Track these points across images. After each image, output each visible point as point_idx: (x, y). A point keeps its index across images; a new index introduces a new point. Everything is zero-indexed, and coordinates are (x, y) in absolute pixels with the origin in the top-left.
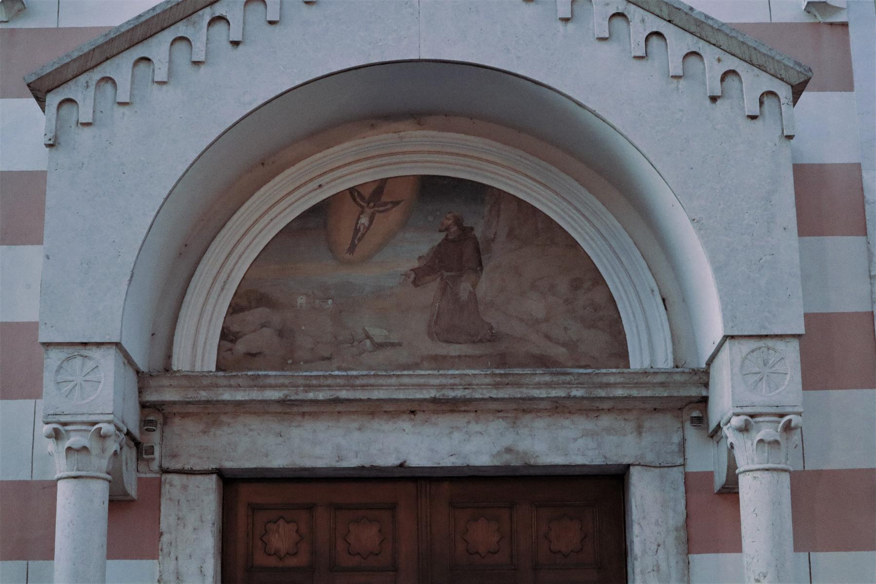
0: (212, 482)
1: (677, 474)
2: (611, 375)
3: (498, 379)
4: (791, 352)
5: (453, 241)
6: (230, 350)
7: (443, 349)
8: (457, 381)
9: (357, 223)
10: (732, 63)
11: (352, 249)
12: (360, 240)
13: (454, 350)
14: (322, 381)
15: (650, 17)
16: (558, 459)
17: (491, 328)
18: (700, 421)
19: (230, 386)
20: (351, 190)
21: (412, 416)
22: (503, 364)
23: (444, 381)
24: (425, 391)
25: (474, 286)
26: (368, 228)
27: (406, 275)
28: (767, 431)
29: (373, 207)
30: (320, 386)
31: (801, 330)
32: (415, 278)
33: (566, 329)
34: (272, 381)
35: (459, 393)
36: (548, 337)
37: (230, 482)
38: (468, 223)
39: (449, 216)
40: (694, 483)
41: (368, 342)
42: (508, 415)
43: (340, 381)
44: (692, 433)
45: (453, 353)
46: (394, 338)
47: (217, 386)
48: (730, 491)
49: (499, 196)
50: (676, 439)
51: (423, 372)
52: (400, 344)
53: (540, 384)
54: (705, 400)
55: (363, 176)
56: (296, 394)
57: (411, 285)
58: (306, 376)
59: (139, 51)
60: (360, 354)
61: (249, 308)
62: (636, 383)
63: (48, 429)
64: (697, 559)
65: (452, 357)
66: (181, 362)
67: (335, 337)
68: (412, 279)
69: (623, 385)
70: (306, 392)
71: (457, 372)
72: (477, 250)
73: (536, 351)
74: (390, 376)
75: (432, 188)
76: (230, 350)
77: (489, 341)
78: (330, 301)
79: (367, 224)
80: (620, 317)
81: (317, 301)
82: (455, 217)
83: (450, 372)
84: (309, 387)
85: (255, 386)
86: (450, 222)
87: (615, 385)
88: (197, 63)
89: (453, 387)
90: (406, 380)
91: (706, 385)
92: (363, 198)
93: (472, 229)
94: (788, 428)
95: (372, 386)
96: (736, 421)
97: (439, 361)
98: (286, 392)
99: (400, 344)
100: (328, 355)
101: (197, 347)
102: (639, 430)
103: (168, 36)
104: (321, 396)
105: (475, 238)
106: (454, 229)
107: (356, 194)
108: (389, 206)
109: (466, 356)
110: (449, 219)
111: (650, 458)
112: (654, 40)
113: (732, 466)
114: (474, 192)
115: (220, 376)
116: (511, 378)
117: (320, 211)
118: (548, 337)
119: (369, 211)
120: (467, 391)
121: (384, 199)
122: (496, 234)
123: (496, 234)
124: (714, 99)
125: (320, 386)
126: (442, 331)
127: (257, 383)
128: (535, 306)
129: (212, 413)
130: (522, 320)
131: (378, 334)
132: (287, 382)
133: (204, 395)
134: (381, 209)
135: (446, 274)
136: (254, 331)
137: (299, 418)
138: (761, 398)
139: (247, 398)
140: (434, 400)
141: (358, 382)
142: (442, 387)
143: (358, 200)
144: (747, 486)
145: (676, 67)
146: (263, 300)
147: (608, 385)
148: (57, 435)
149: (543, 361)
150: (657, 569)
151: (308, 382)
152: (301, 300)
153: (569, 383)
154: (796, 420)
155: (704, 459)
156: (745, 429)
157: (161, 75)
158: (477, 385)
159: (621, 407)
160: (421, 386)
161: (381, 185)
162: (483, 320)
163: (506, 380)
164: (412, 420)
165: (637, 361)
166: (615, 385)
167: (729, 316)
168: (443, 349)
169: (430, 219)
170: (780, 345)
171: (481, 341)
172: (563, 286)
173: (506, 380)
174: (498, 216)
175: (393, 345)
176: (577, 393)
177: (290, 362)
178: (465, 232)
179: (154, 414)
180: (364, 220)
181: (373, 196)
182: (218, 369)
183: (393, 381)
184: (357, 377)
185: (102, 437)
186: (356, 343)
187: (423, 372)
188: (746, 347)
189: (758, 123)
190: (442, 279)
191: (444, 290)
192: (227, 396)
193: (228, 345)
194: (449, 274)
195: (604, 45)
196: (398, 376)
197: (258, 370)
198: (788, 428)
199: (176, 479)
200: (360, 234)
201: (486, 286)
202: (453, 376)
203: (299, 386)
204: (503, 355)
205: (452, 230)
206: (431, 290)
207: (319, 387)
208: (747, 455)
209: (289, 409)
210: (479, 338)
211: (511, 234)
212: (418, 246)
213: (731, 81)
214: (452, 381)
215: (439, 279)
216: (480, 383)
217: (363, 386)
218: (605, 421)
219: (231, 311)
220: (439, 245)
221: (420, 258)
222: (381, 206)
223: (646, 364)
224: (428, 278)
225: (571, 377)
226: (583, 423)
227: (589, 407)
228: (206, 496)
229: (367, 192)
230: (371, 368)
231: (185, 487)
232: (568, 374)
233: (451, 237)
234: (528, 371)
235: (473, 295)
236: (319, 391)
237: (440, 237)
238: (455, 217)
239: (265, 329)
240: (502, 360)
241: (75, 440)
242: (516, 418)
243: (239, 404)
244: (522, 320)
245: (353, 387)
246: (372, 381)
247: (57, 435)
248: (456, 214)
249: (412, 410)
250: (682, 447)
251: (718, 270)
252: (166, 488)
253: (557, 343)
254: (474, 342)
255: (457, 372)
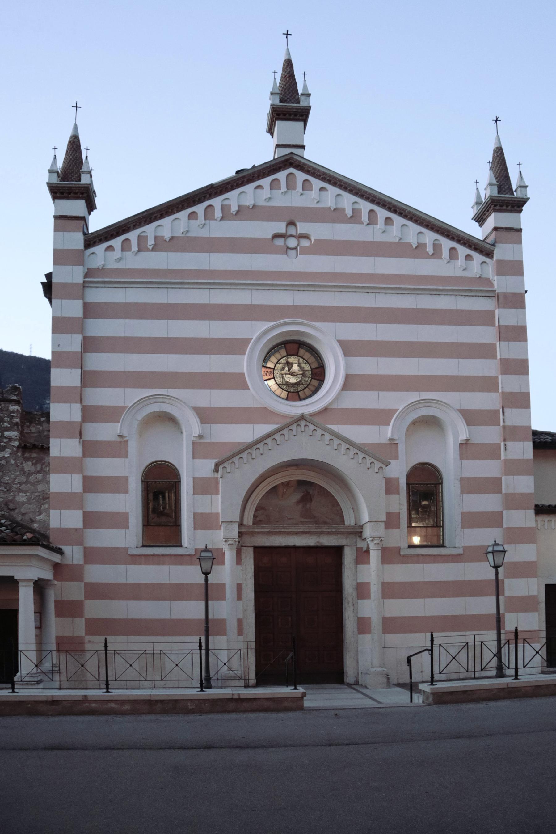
0: (252, 549)
1: (355, 548)
2: (341, 526)
4: (383, 525)
10: (373, 460)
11: (282, 497)
13: (305, 520)
15: (355, 449)
16: (329, 544)
18: (361, 537)
22: (316, 524)
28: (377, 541)
31: (385, 520)
35: (308, 530)
37: (257, 549)
40: (359, 550)
44: (358, 539)
48: (367, 551)
50: (355, 540)
54: (361, 532)
55: (285, 480)
59: (240, 456)
63: (224, 540)
64: (359, 566)
66: (245, 523)
75: (301, 483)
84: (274, 529)
88: (253, 459)
91: (362, 529)
94: (381, 541)
96: (370, 539)
97: (303, 523)
101: (249, 520)
102: (347, 538)
103: (246, 452)
104: (277, 530)
111: (349, 544)
112: (356, 455)
113: (368, 547)
114: (310, 484)
117: (274, 488)
124: (368, 468)
127: (263, 528)
129: (252, 534)
133: (251, 530)
138: (376, 534)
140: (302, 532)
144: (371, 552)
145: (360, 461)
148: (226, 541)
149: (326, 523)
150: (350, 568)
154: (383, 539)
155: (361, 545)
156: (372, 541)
157: (245, 461)
159: (342, 533)
161: (289, 482)
165: (347, 523)
167: (370, 515)
170: (380, 523)
176: (334, 530)
178: (308, 493)
179: (241, 534)
181: (287, 485)
182: (253, 524)
185: (235, 541)
188: (373, 523)
189: (378, 474)
192: (256, 530)
195: (345, 456)
198: (381, 541)
199: (245, 548)
206: (301, 506)
208: (372, 546)
209: (269, 533)
212: (297, 496)
213: (372, 464)
216: (312, 528)
218: (339, 536)
226: (335, 537)
227: (336, 533)
228: (251, 551)
231: (246, 550)
237: (302, 494)
240: (316, 523)
241: (230, 542)
243: (258, 532)
247: (226, 541)
249: (297, 533)
250: (356, 543)
251: (368, 507)
252: (242, 550)
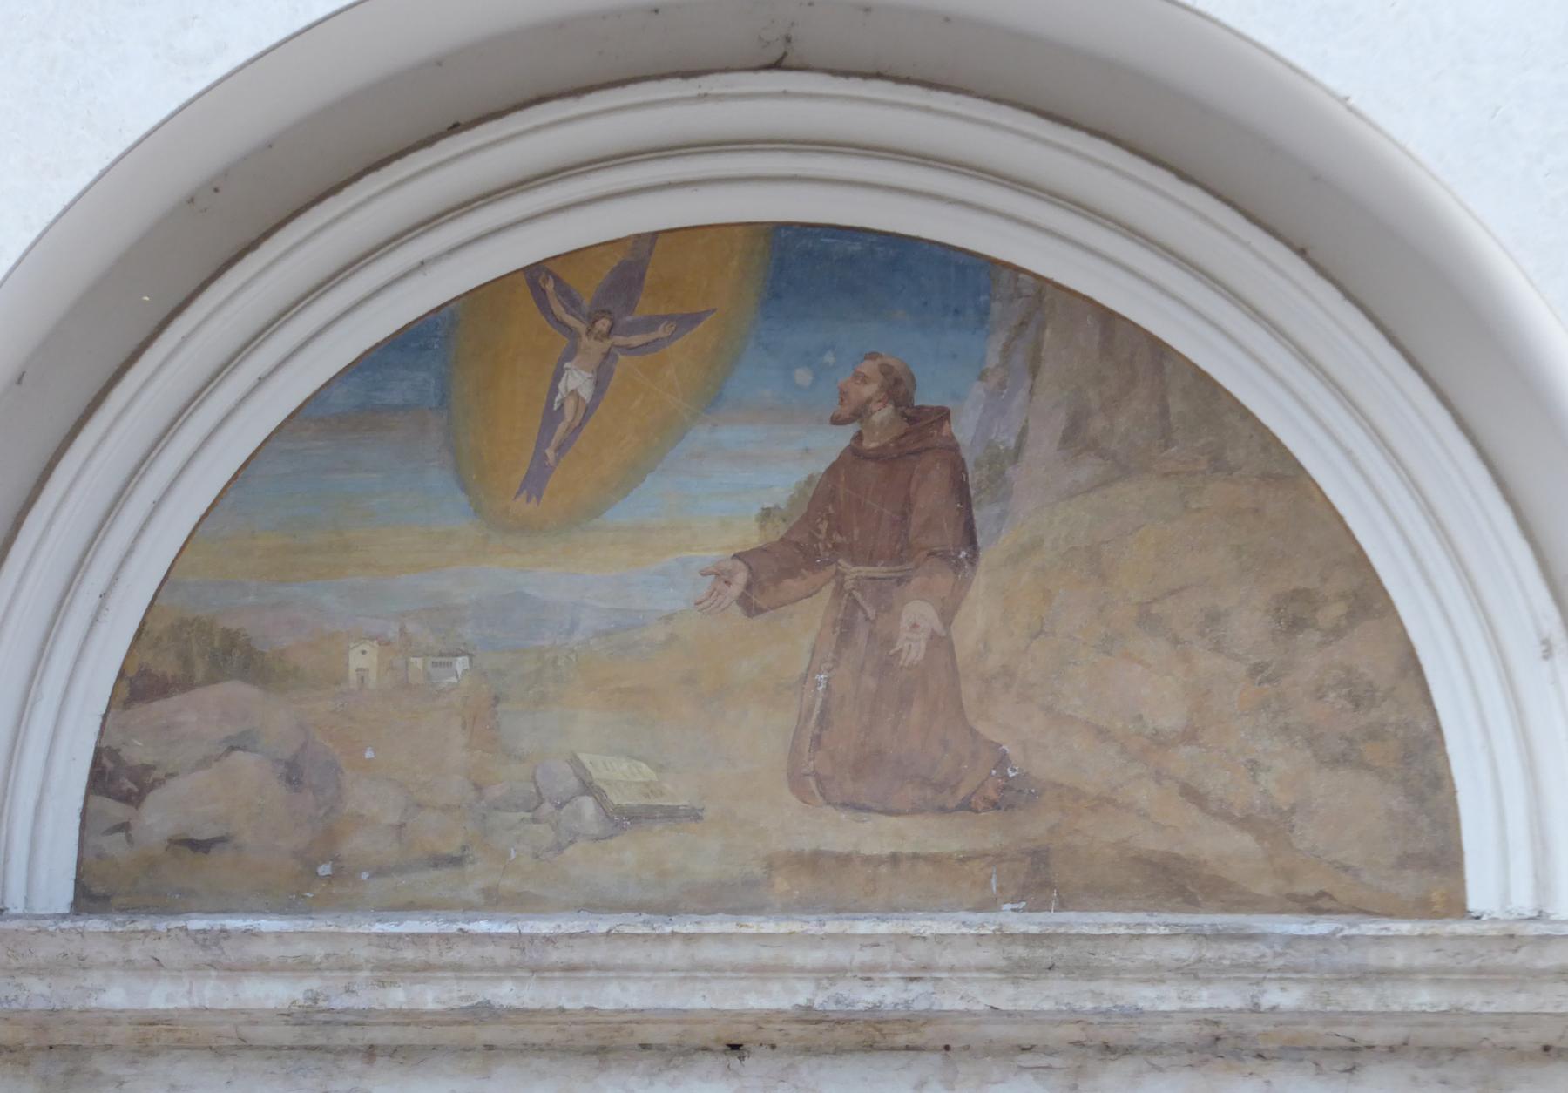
3: (1020, 951)
5: (877, 457)
6: (124, 827)
7: (839, 833)
8: (886, 956)
9: (554, 390)
11: (534, 483)
12: (561, 449)
13: (873, 836)
14: (434, 954)
17: (1003, 761)
19: (129, 965)
20: (535, 275)
21: (734, 1061)
23: (840, 956)
24: (775, 987)
25: (947, 615)
26: (590, 409)
27: (721, 575)
29: (609, 334)
30: (428, 967)
32: (748, 587)
33: (1254, 766)
34: (272, 952)
35: (888, 995)
36: (1193, 795)
38: (926, 397)
39: (868, 367)
41: (588, 806)
42: (1056, 1062)
43: (501, 954)
45: (872, 848)
46: (678, 794)
47: (83, 964)
49: (1044, 296)
51: (770, 927)
52: (695, 815)
53: (1158, 967)
56: (349, 991)
57: (737, 610)
58: (381, 936)
60: (559, 848)
61: (186, 683)
62: (1480, 970)
65: (868, 860)
67: (478, 787)
68: (736, 589)
69: (1437, 976)
70: (382, 983)
71: (883, 928)
72: (960, 490)
73: (1150, 842)
74: (661, 938)
75: (813, 269)
76: (124, 827)
77: (995, 805)
78: (461, 664)
79: (586, 393)
80: (1438, 729)
81: (418, 663)
82: (886, 371)
83: (863, 927)
84: (389, 972)
85: (211, 966)
86: (869, 390)
87: (1406, 975)
89: (868, 974)
90: (710, 952)
92: (573, 303)
93: (943, 415)
95: (600, 968)
97: (824, 879)
98: (314, 983)
99: (695, 815)
100: (451, 848)
105: (954, 447)
106: (882, 414)
107: (550, 286)
108: (662, 332)
109: (915, 857)
110: (865, 380)
115: (96, 934)
116: (1061, 949)
118: (1193, 795)
119: (593, 348)
120: (916, 988)
121: (646, 306)
122: (1023, 433)
123: (1023, 433)
125: (428, 967)
126: (841, 767)
127: (218, 958)
128: (1154, 691)
130: (1103, 734)
131: (625, 778)
132: (319, 951)
134: (636, 340)
135: (854, 572)
136: (205, 763)
137: (355, 1065)
139: (184, 1003)
141: (555, 956)
142: (833, 973)
143: (558, 309)
146: (236, 657)
147: (1384, 974)
149: (1174, 882)
151: (388, 955)
152: (362, 659)
153: (1254, 967)
158: (952, 969)
160: (763, 972)
162: (974, 733)
163: (1042, 954)
164: (737, 1075)
166: (1406, 975)
168: (839, 833)
169: (803, 376)
171: (966, 806)
172: (1249, 624)
173: (1042, 954)
174: (1034, 368)
175: (671, 814)
177: (325, 869)
178: (922, 427)
180: (577, 380)
181: (611, 294)
183: (673, 954)
184: (550, 940)
186: (547, 808)
187: (770, 927)
190: (839, 590)
191: (845, 629)
192: (116, 996)
193: (117, 811)
194: (865, 570)
196: (689, 938)
197: (227, 911)
200: (562, 428)
201: (985, 613)
202: (873, 942)
203: (354, 968)
204: (1039, 857)
205: (877, 418)
206: (806, 619)
207: (425, 970)
210: (962, 792)
211: (1075, 438)
214: (866, 956)
215: (827, 591)
217: (571, 968)
219: (125, 692)
220: (833, 470)
221: (767, 514)
222: (631, 329)
223: (1523, 902)
224: (792, 585)
225: (1263, 948)
229: (587, 288)
230: (595, 906)
232: (1251, 937)
233: (870, 444)
234: (1115, 921)
235: (941, 643)
236: (425, 981)
238: (886, 371)
239: (238, 756)
240: (1040, 878)
242: (1079, 1072)
244: (1103, 734)
245: (538, 970)
246: (599, 954)
248: (891, 361)
253: (1227, 817)
254: (943, 810)
255: (883, 928)
